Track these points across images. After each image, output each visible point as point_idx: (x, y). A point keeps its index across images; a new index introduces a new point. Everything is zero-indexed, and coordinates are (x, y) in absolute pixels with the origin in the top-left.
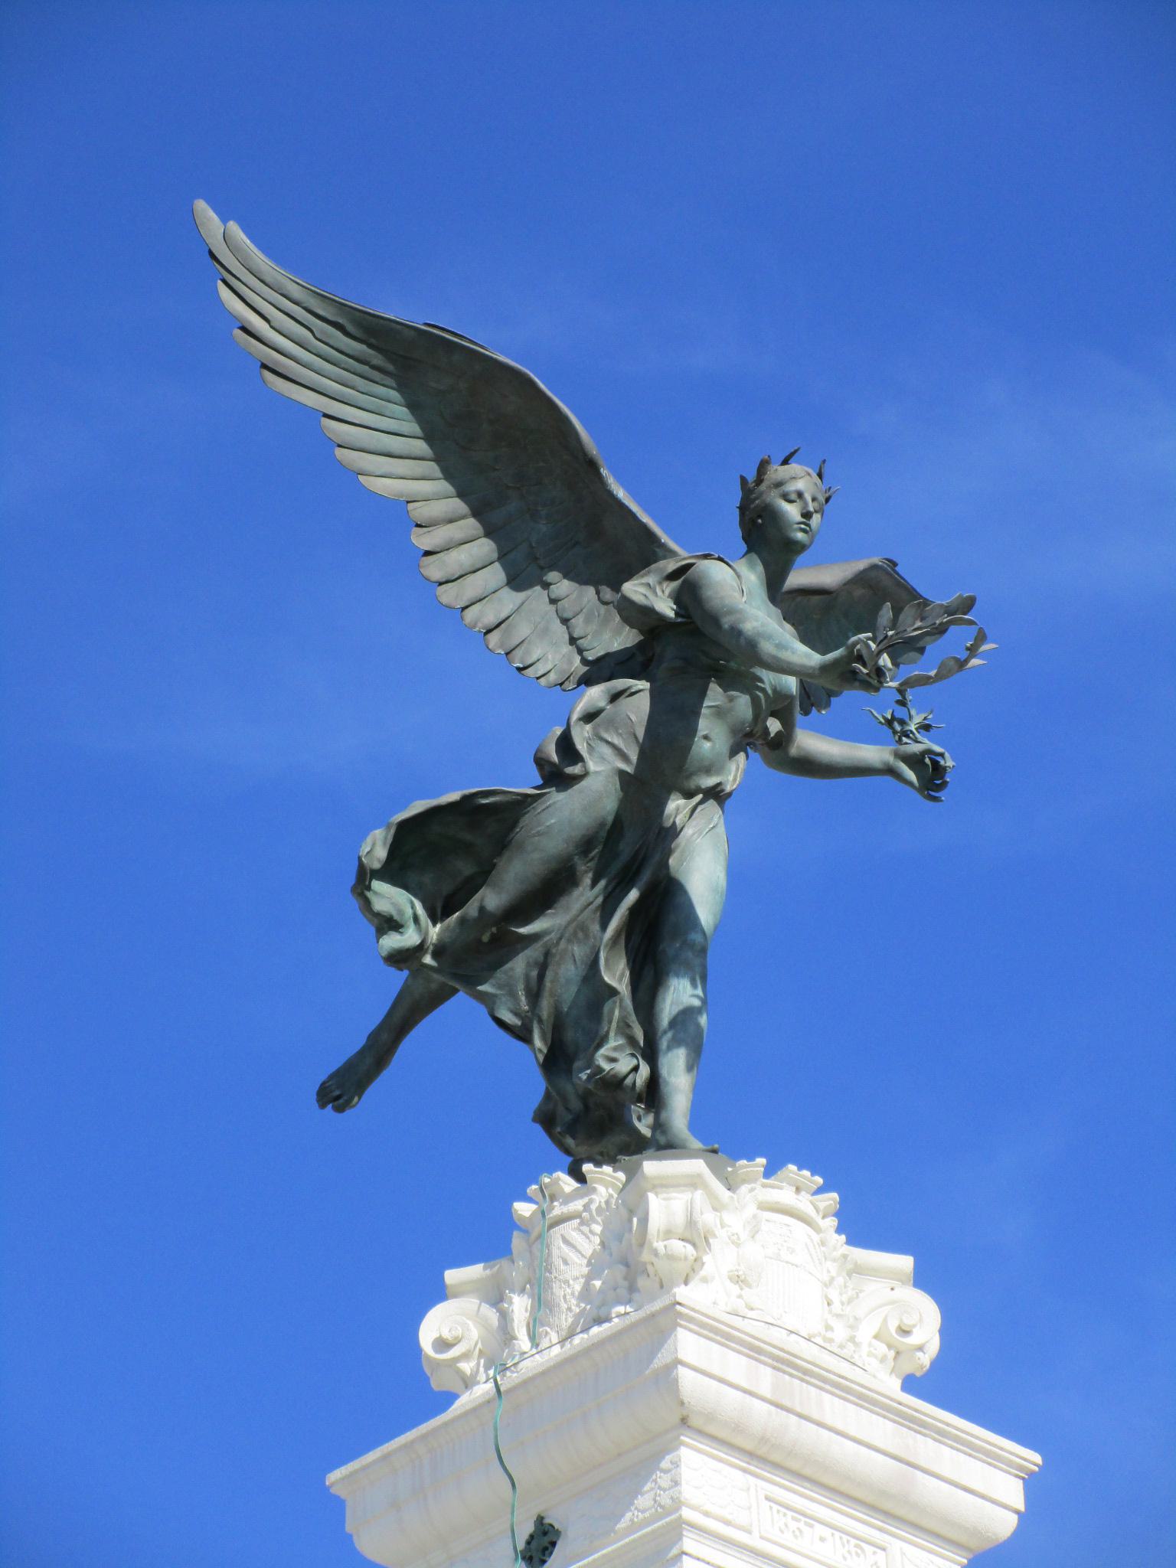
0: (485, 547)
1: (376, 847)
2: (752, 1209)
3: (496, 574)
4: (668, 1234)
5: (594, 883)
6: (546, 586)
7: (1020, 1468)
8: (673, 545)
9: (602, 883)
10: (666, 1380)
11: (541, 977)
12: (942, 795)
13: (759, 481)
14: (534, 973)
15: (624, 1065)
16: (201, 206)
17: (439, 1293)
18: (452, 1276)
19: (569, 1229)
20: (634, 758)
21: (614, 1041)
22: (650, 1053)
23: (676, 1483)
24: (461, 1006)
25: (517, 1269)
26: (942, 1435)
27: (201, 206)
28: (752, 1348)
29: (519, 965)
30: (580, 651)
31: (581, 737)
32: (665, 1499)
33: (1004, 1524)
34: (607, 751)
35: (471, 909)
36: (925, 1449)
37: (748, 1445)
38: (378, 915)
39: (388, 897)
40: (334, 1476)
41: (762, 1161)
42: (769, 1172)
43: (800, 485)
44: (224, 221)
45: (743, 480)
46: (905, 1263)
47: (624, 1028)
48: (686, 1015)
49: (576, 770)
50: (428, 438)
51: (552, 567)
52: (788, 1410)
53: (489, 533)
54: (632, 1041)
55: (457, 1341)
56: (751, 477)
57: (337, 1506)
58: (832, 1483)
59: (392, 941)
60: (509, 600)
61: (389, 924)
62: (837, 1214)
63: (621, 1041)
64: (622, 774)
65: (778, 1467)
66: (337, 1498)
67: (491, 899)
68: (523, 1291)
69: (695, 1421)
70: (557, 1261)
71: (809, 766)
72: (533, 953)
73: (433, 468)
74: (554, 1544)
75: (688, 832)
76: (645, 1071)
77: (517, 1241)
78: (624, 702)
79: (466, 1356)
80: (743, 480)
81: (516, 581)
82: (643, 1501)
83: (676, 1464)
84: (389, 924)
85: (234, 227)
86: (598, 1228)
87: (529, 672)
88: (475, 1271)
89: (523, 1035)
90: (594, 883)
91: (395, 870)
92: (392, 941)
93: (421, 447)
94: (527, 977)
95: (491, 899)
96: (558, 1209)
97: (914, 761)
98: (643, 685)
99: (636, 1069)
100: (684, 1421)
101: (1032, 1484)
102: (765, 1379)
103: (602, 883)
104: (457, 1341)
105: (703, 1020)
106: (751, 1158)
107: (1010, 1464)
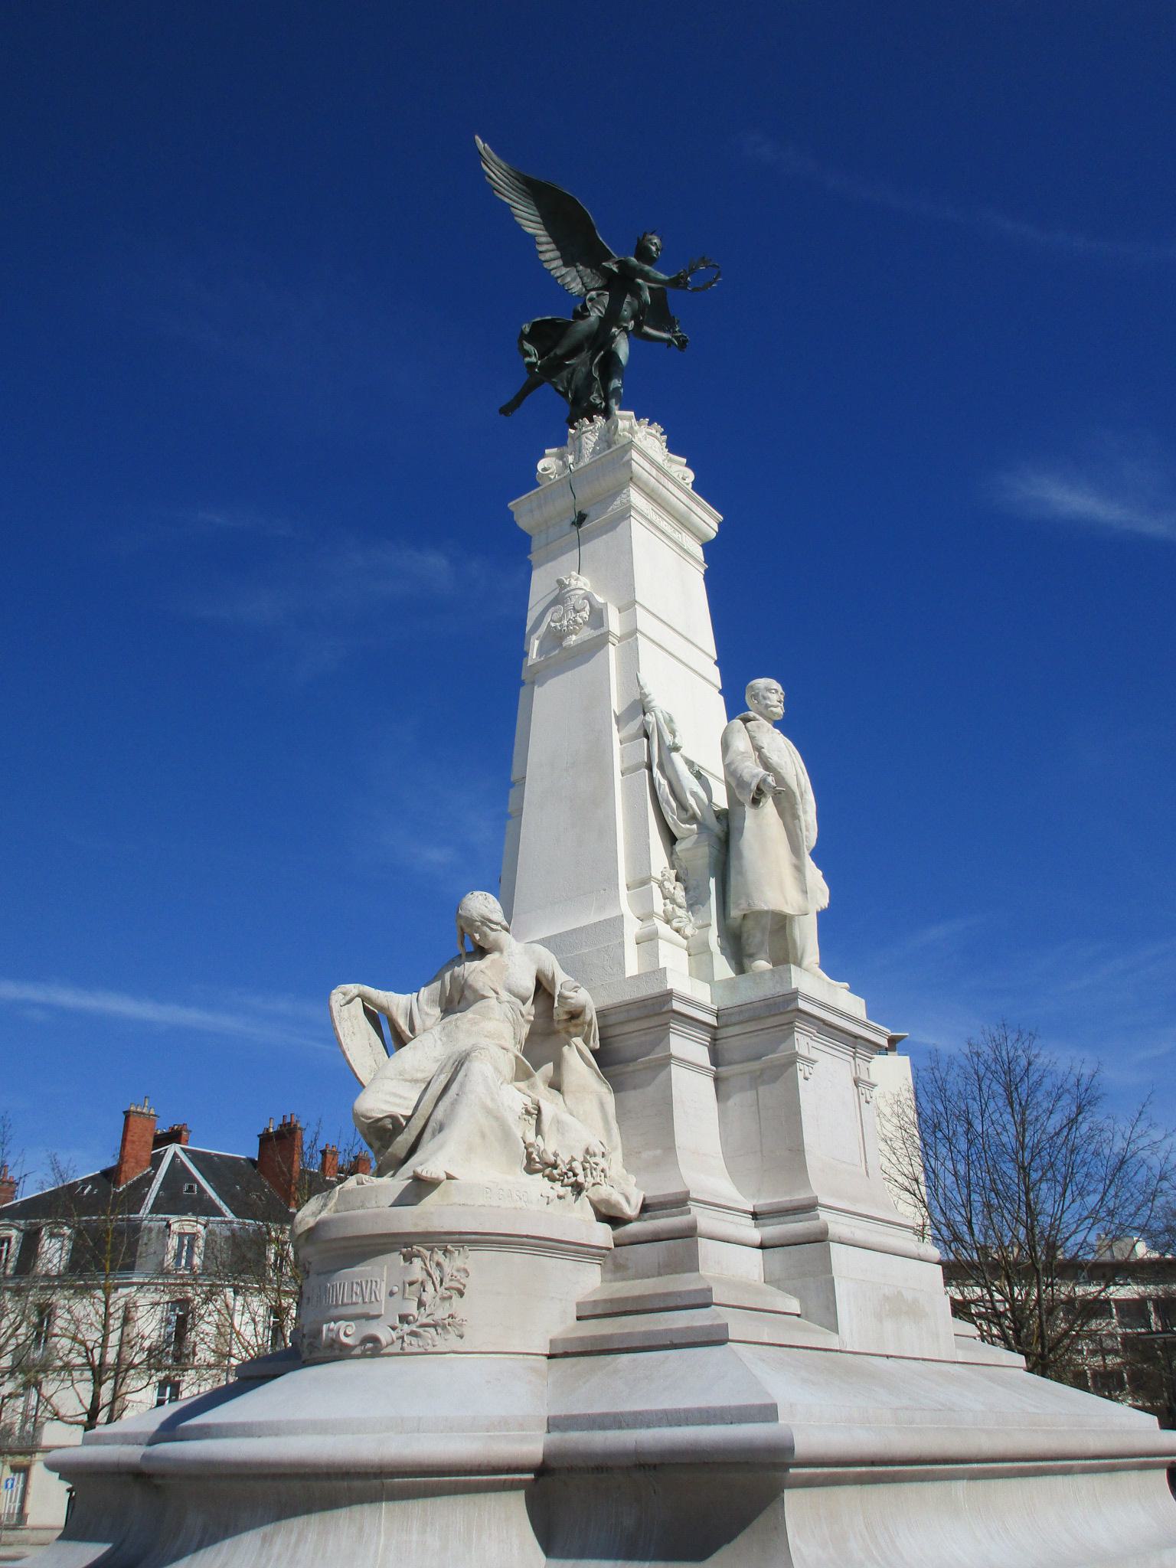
0: (557, 254)
1: (526, 328)
2: (644, 433)
3: (559, 262)
4: (624, 430)
5: (587, 352)
6: (576, 267)
7: (718, 520)
8: (615, 255)
9: (591, 351)
10: (628, 464)
11: (572, 376)
12: (685, 350)
13: (643, 239)
14: (569, 376)
15: (598, 401)
16: (477, 137)
17: (542, 456)
18: (547, 451)
19: (588, 435)
20: (604, 312)
21: (595, 395)
22: (606, 399)
23: (629, 496)
24: (546, 388)
25: (570, 448)
26: (698, 504)
27: (477, 137)
28: (651, 461)
29: (565, 374)
30: (585, 287)
31: (589, 305)
32: (625, 501)
33: (713, 535)
34: (596, 311)
35: (552, 354)
36: (694, 506)
37: (648, 491)
38: (525, 350)
39: (528, 346)
40: (510, 504)
41: (648, 420)
42: (650, 424)
43: (656, 241)
44: (484, 143)
45: (638, 239)
46: (684, 461)
47: (598, 391)
48: (617, 389)
49: (587, 314)
50: (541, 217)
51: (578, 261)
52: (660, 483)
53: (558, 249)
54: (600, 395)
55: (550, 468)
56: (641, 238)
57: (512, 514)
58: (669, 509)
59: (527, 359)
60: (564, 270)
61: (528, 354)
62: (522, 683)
63: (596, 395)
64: (600, 317)
65: (655, 501)
66: (510, 511)
67: (559, 351)
68: (571, 454)
69: (634, 480)
70: (583, 443)
71: (647, 337)
72: (570, 370)
73: (542, 226)
74: (585, 519)
75: (618, 338)
76: (604, 404)
77: (569, 441)
78: (602, 297)
79: (551, 473)
80: (638, 239)
81: (566, 265)
82: (617, 502)
83: (629, 491)
84: (528, 354)
85: (486, 145)
86: (597, 434)
87: (570, 291)
88: (555, 450)
89: (565, 395)
90: (587, 352)
91: (530, 338)
92: (527, 359)
93: (539, 219)
94: (567, 377)
95: (559, 351)
96: (584, 429)
97: (677, 338)
98: (608, 293)
99: (601, 403)
100: (631, 479)
101: (720, 525)
102: (654, 472)
103: (591, 351)
104: (550, 468)
105: (622, 391)
106: (644, 418)
107: (715, 517)
